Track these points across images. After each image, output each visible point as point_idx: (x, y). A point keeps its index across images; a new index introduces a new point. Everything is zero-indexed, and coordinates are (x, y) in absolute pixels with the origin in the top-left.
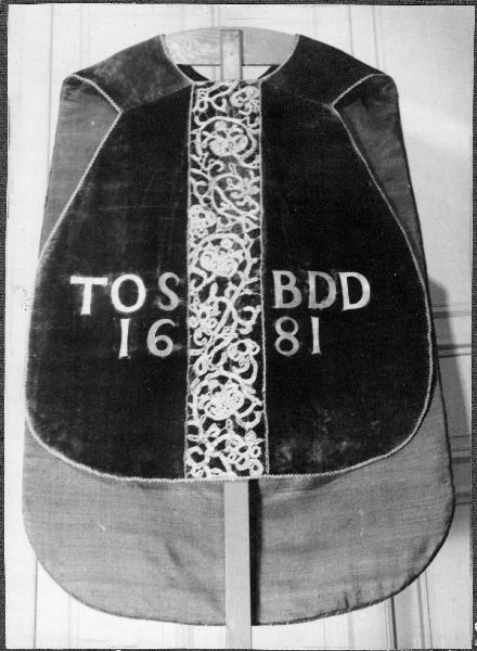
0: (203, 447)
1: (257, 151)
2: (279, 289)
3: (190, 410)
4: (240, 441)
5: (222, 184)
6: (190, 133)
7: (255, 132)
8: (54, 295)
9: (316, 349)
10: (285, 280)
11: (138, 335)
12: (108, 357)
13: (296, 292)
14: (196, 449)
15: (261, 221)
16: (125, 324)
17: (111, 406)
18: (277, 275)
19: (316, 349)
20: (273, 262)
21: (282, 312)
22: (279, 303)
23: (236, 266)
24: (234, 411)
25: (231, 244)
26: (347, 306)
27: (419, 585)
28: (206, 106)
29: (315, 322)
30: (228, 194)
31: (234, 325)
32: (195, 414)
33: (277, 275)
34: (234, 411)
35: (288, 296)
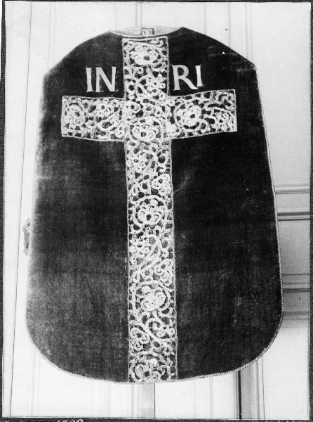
1: (172, 305)
2: (176, 77)
4: (154, 80)
5: (143, 82)
6: (128, 209)
7: (171, 290)
8: (50, 125)
10: (181, 72)
12: (80, 179)
15: (168, 51)
17: (91, 343)
18: (175, 68)
20: (173, 60)
23: (155, 134)
24: (158, 307)
25: (156, 203)
27: (257, 365)
28: (137, 191)
30: (146, 87)
31: (159, 253)
33: (175, 68)
34: (158, 307)
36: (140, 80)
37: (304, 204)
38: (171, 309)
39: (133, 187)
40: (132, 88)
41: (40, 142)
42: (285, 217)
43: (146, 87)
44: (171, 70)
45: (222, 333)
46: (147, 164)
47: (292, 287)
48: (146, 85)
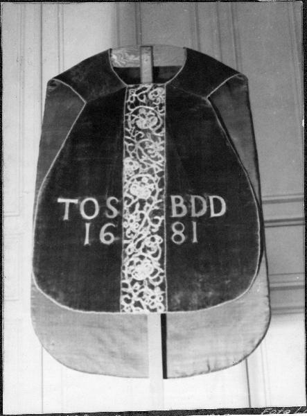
0: (131, 295)
1: (163, 126)
2: (174, 206)
3: (124, 274)
4: (151, 292)
9: (195, 240)
10: (178, 201)
11: (95, 233)
13: (184, 207)
14: (127, 296)
16: (88, 226)
17: (79, 271)
18: (173, 198)
19: (195, 240)
20: (172, 190)
21: (176, 219)
22: (174, 214)
26: (213, 215)
28: (134, 99)
29: (194, 224)
31: (149, 227)
32: (126, 276)
33: (173, 198)
35: (179, 210)
36: (138, 293)
37: (298, 211)
38: (161, 278)
39: (128, 247)
40: (128, 301)
41: (41, 340)
42: (282, 223)
43: (146, 151)
44: (169, 201)
45: (211, 263)
46: (140, 223)
47: (292, 284)
48: (146, 148)
